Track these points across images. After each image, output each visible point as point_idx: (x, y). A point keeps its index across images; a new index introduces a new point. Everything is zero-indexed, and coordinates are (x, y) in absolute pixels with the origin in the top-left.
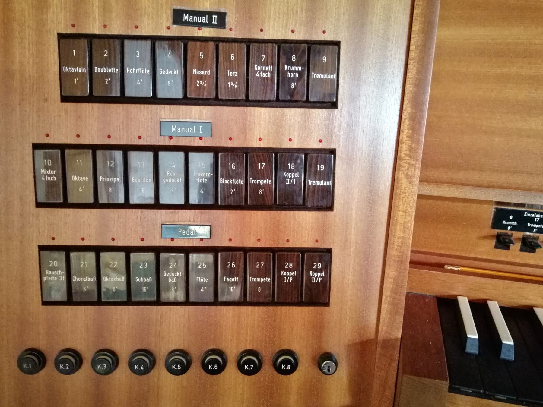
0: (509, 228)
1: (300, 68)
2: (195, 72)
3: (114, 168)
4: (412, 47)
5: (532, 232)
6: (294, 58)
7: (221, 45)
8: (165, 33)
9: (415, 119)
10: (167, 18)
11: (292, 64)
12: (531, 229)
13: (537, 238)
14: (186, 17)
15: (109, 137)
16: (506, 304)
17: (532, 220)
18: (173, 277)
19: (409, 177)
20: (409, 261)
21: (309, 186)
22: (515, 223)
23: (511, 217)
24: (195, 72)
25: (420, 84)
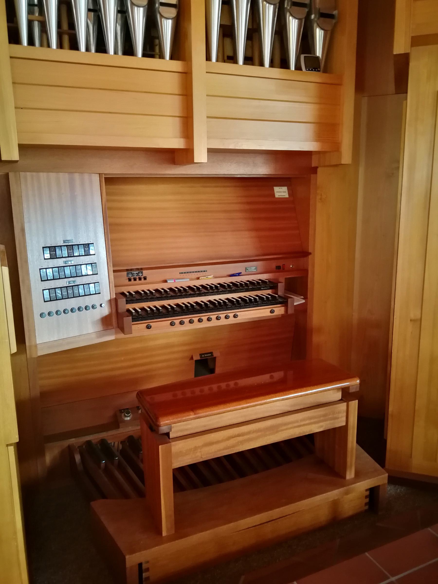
0: (130, 276)
1: (88, 248)
2: (69, 251)
3: (334, 162)
4: (106, 243)
5: (135, 276)
6: (86, 247)
7: (84, 245)
8: (62, 245)
9: (109, 255)
10: (62, 242)
11: (86, 248)
12: (134, 276)
13: (136, 277)
14: (66, 242)
15: (54, 265)
16: (140, 308)
17: (134, 274)
18: (70, 292)
19: (110, 266)
20: (114, 286)
21: (64, 295)
22: (131, 275)
23: (130, 274)
24: (69, 251)
25: (109, 249)
